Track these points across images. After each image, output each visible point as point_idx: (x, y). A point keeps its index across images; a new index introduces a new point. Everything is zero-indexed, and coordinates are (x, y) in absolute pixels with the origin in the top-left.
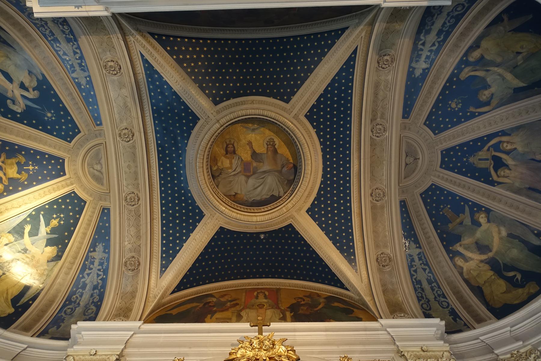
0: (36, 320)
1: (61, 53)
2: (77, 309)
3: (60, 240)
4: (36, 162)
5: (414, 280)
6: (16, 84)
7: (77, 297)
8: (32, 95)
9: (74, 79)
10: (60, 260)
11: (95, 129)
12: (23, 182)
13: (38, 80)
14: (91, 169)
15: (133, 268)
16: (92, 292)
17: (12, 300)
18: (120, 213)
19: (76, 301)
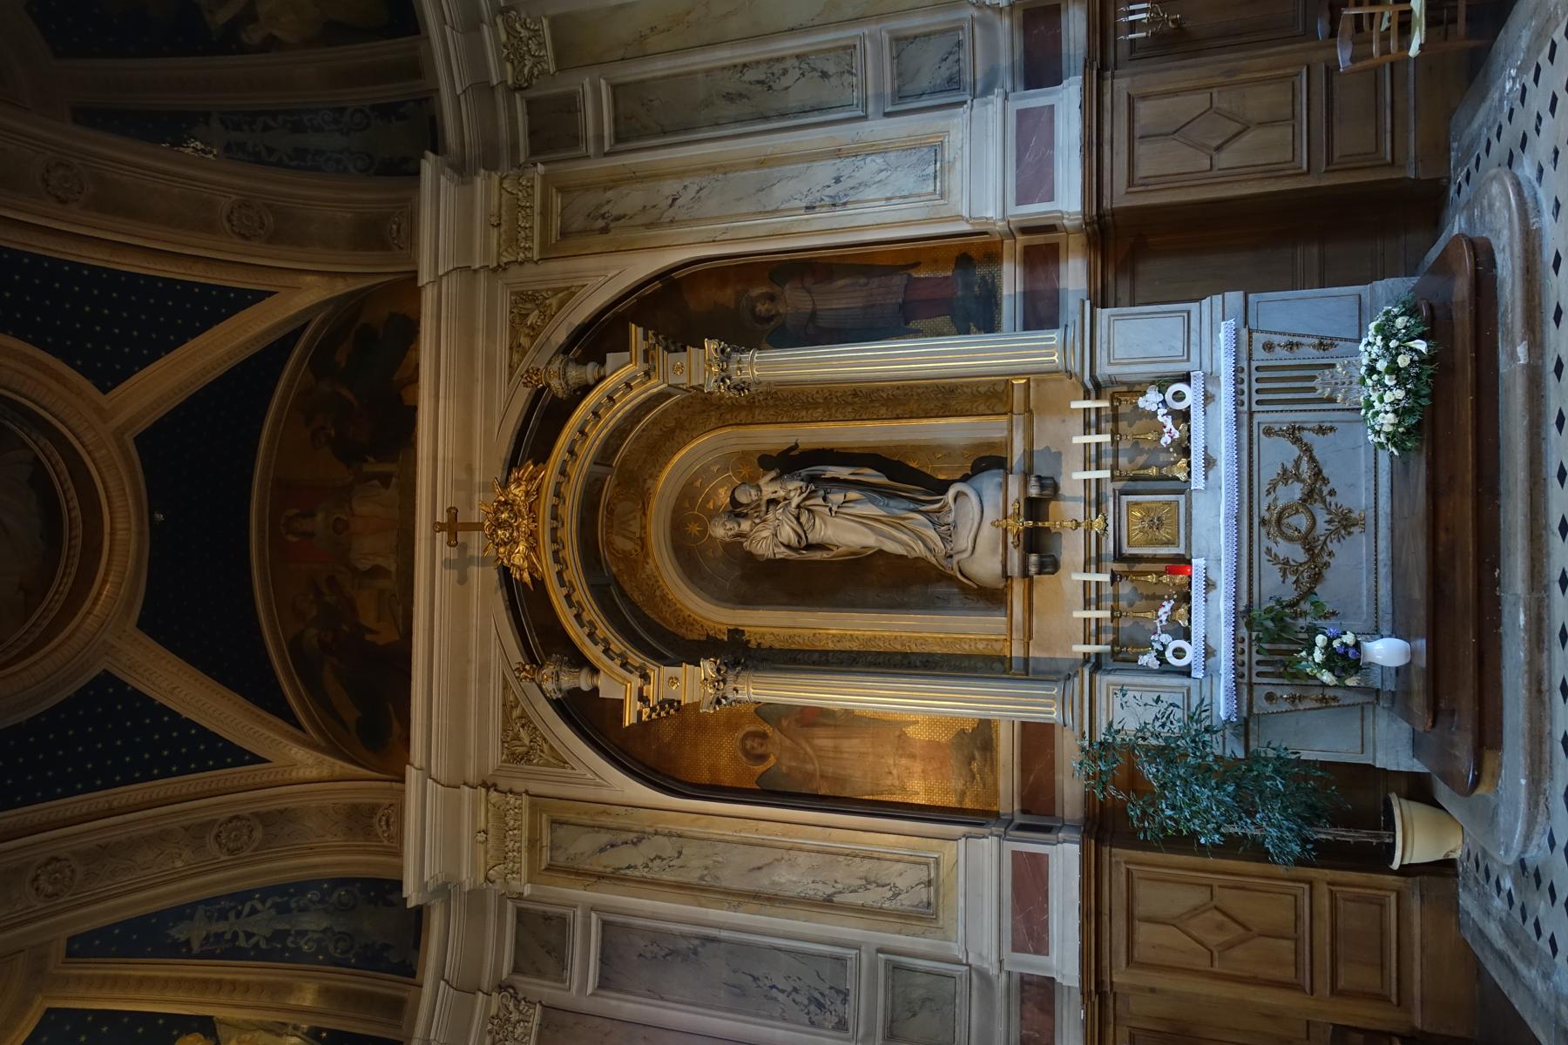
5: (294, 163)
10: (211, 1018)
18: (96, 902)
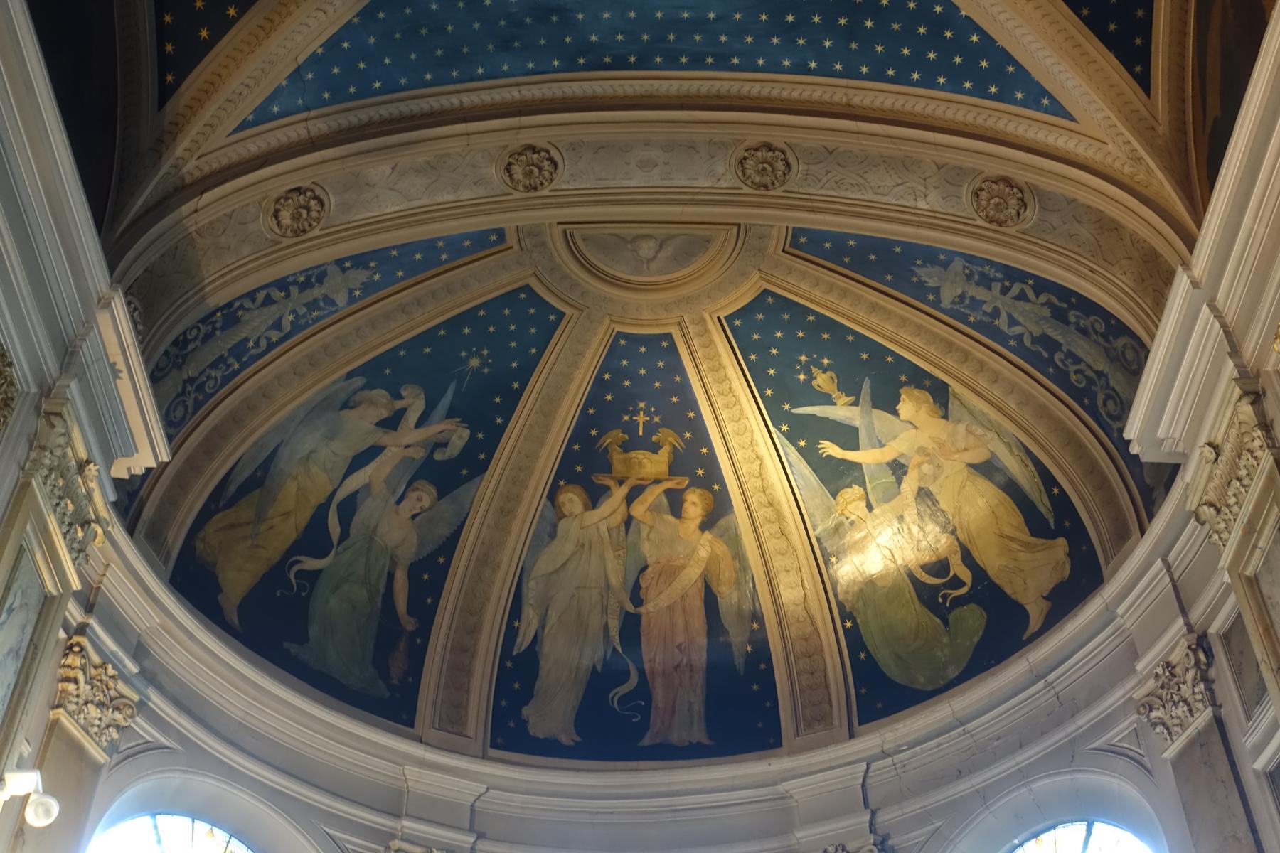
0: (1110, 500)
1: (275, 336)
2: (1112, 383)
3: (885, 380)
4: (626, 402)
6: (384, 438)
7: (1076, 372)
8: (415, 403)
9: (352, 300)
11: (516, 247)
12: (685, 440)
13: (369, 386)
14: (653, 266)
15: (1013, 202)
16: (1072, 328)
17: (1033, 534)
19: (1087, 378)
